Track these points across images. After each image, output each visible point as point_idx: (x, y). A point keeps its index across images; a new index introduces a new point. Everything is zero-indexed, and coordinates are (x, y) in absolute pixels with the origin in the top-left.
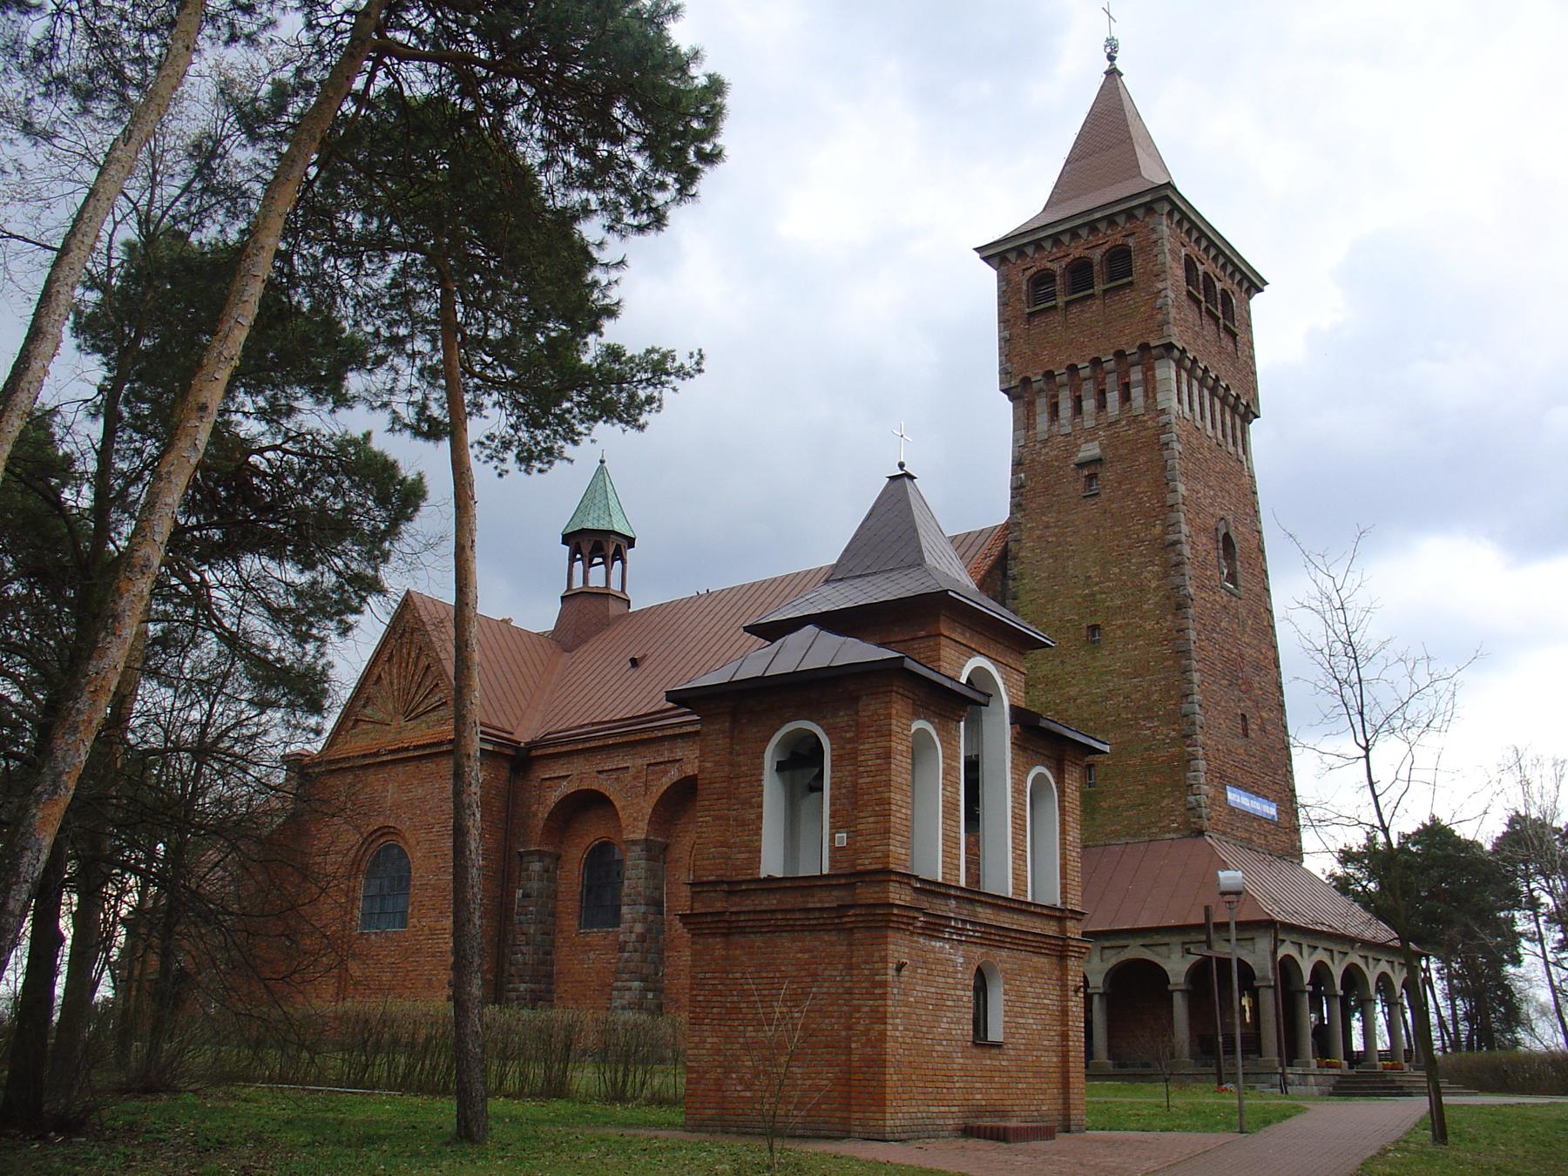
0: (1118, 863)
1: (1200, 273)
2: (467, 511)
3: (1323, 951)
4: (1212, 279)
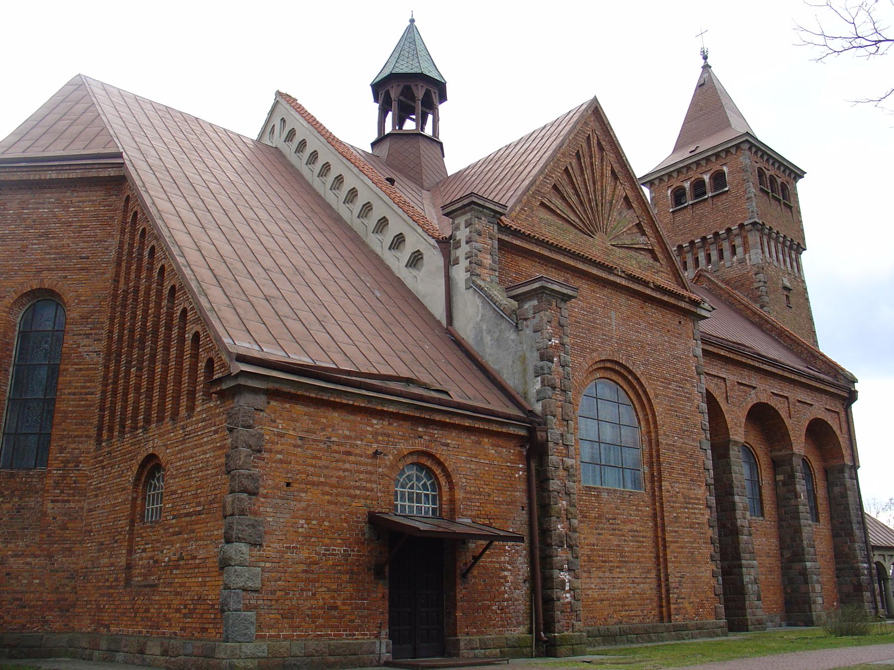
0: (727, 392)
1: (779, 184)
2: (381, 389)
3: (879, 557)
4: (763, 171)
